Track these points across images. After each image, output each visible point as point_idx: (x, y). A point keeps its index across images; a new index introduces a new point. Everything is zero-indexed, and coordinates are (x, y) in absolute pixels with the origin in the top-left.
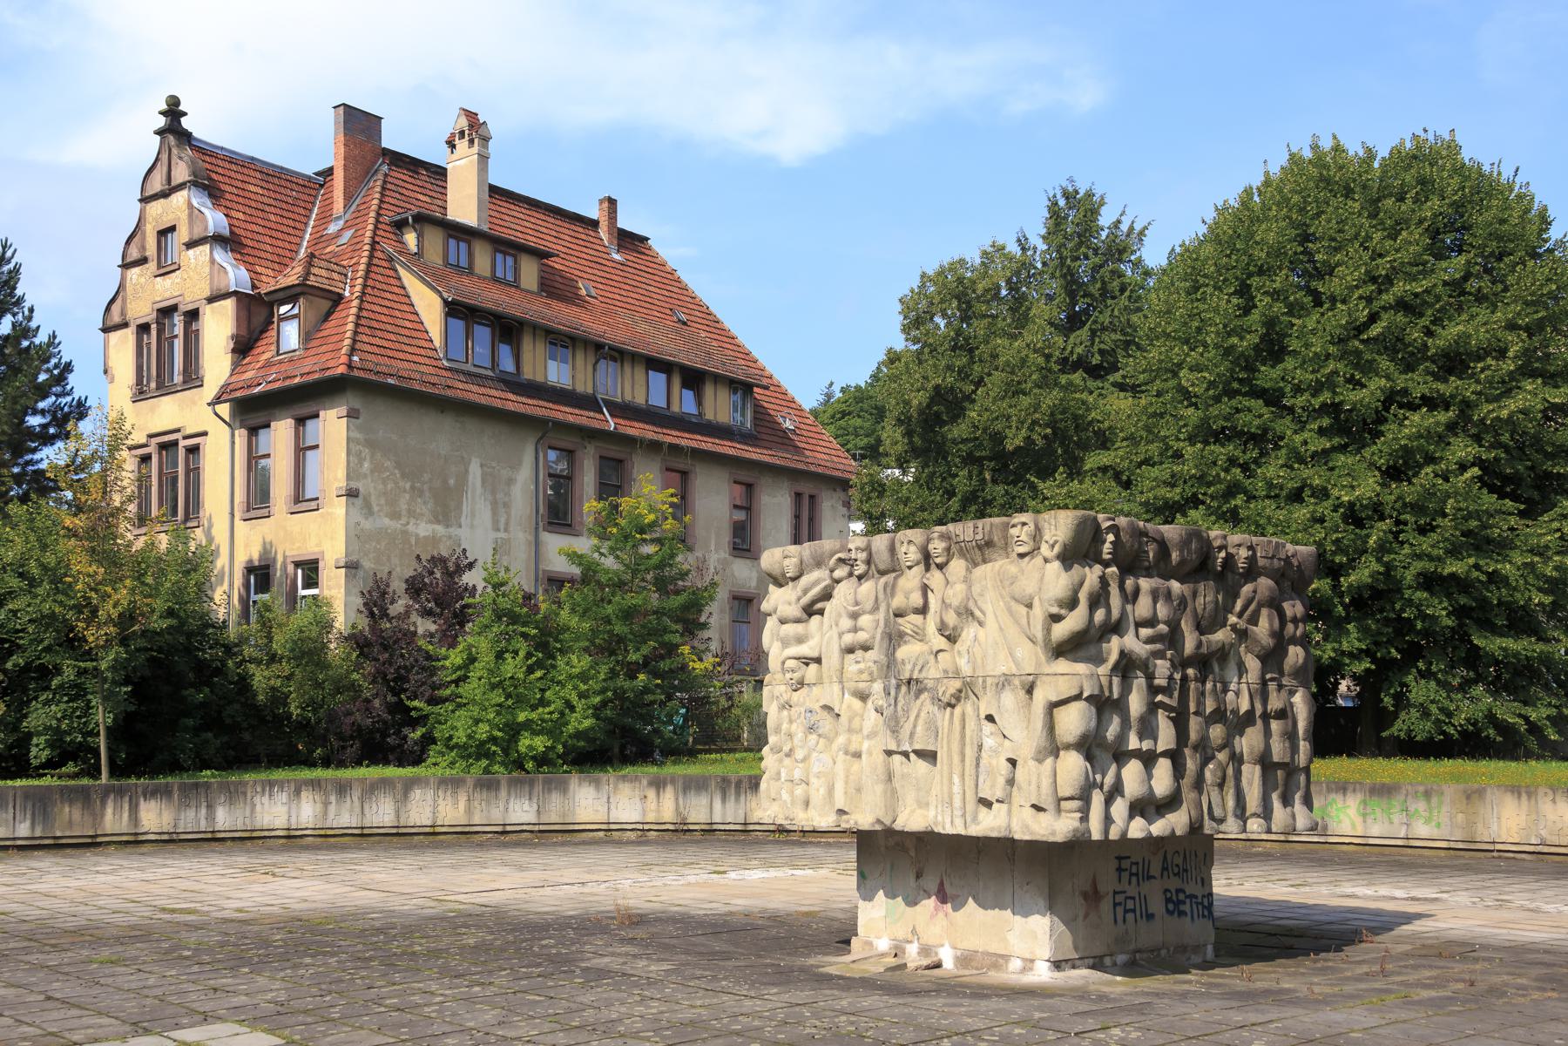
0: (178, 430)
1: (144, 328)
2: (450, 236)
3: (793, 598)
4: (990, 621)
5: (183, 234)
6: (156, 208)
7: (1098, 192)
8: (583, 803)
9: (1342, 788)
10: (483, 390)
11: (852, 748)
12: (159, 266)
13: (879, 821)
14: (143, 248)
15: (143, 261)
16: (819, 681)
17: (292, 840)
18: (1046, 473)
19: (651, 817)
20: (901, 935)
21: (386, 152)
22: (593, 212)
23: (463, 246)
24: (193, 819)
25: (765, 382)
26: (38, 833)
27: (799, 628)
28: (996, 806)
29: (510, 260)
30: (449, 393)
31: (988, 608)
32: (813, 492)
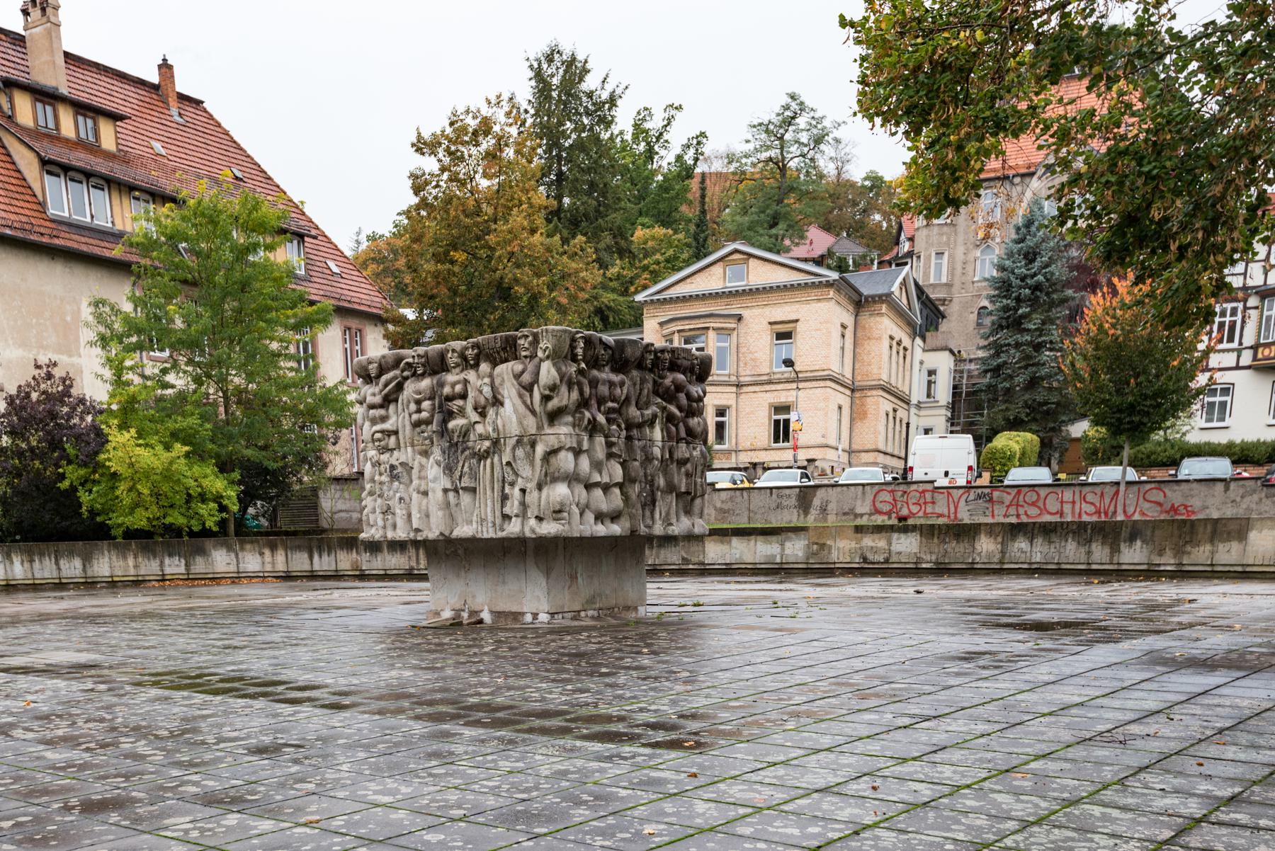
3: (377, 390)
4: (507, 403)
8: (219, 558)
10: (83, 240)
11: (422, 489)
13: (442, 534)
16: (398, 447)
18: (694, 408)
19: (268, 568)
20: (458, 606)
22: (154, 78)
25: (314, 232)
27: (382, 412)
28: (514, 519)
29: (90, 122)
30: (56, 241)
31: (506, 393)
32: (360, 327)
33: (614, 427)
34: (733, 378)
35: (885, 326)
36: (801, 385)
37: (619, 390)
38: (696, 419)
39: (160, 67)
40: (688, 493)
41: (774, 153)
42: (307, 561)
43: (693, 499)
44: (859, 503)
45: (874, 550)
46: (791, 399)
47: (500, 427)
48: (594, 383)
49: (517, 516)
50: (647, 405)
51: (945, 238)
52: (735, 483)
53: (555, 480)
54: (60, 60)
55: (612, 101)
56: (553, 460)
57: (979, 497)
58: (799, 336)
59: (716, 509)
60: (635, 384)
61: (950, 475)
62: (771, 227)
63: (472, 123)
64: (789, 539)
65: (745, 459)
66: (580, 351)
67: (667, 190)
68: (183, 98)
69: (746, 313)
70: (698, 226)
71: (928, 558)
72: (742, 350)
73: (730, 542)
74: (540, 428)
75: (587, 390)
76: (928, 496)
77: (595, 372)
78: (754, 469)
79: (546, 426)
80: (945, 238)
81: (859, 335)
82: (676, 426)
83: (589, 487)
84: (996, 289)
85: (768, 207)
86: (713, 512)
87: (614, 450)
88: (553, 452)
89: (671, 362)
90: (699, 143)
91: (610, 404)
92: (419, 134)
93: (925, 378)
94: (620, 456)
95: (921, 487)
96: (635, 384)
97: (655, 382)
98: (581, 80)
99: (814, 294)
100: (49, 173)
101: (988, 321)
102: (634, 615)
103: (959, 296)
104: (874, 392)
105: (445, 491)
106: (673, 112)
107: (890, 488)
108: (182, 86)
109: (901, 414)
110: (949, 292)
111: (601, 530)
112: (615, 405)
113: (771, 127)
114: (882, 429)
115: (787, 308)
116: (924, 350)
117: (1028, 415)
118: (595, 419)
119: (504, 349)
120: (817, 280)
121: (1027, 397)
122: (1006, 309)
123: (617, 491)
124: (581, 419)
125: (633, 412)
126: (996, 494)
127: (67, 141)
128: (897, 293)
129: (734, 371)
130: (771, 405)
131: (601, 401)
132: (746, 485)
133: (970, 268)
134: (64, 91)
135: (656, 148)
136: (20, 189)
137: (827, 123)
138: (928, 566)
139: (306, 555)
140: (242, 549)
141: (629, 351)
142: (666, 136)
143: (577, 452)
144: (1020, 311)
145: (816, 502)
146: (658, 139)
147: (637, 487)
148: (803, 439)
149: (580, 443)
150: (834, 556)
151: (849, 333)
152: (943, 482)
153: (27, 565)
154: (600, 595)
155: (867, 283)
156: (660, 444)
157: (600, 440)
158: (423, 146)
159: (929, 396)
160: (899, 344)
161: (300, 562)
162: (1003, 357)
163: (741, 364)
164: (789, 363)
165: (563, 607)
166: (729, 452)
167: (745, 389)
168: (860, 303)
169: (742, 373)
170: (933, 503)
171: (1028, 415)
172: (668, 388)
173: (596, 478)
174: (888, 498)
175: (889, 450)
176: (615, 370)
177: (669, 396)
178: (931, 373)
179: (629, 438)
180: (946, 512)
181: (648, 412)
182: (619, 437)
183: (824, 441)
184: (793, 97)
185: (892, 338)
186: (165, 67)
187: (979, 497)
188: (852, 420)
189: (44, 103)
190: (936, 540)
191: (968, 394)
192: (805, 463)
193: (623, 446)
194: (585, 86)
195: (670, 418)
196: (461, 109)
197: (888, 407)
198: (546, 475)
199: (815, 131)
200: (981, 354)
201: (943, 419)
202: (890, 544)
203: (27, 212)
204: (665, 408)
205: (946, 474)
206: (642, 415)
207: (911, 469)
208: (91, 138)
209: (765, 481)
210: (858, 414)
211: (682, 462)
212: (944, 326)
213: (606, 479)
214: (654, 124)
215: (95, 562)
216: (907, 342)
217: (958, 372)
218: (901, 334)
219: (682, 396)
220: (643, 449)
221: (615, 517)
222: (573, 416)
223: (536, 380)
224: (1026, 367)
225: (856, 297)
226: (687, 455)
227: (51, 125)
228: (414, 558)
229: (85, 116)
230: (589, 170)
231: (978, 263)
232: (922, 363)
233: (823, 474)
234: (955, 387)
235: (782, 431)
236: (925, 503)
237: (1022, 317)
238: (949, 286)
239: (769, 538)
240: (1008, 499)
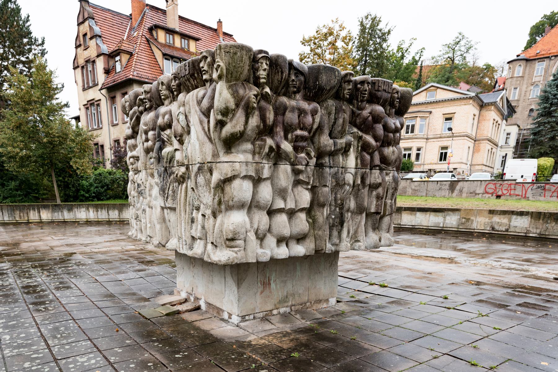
0: (94, 99)
1: (83, 67)
2: (167, 33)
5: (89, 36)
6: (82, 27)
7: (378, 16)
9: (319, 142)
12: (85, 47)
14: (80, 41)
15: (80, 45)
17: (88, 223)
18: (390, 138)
21: (147, 5)
22: (215, 27)
23: (171, 36)
24: (103, 215)
26: (11, 219)
33: (303, 155)
34: (425, 136)
35: (492, 115)
36: (454, 138)
37: (309, 119)
38: (391, 149)
39: (218, 22)
40: (377, 213)
41: (451, 55)
43: (382, 218)
44: (478, 188)
45: (500, 224)
46: (448, 144)
47: (189, 155)
48: (281, 110)
49: (200, 239)
50: (342, 134)
51: (518, 82)
52: (421, 178)
53: (230, 208)
54: (177, 18)
55: (389, 32)
56: (227, 189)
57: (539, 187)
58: (455, 119)
59: (412, 189)
60: (329, 114)
61: (524, 177)
62: (446, 82)
63: (325, 31)
64: (449, 215)
65: (426, 168)
66: (262, 74)
67: (407, 69)
68: (225, 34)
69: (433, 110)
70: (418, 81)
71: (535, 231)
72: (430, 125)
73: (416, 214)
74: (215, 155)
75: (270, 116)
76: (513, 187)
77: (284, 99)
78: (430, 172)
79: (221, 153)
80: (518, 82)
81: (480, 119)
82: (371, 155)
83: (271, 213)
84: (542, 100)
85: (445, 75)
86: (410, 190)
87: (301, 177)
88: (228, 180)
89: (370, 94)
90: (422, 52)
91: (299, 132)
92: (304, 38)
93: (505, 136)
94: (308, 183)
95: (510, 182)
96: (329, 114)
97: (353, 113)
98: (378, 25)
99: (465, 101)
100: (166, 59)
101: (535, 114)
102: (325, 305)
103: (521, 104)
104: (484, 142)
105: (163, 208)
106: (413, 41)
107: (494, 182)
108: (225, 30)
109: (494, 150)
110: (518, 103)
111: (283, 252)
112: (305, 133)
113: (450, 45)
114: (486, 156)
115: (451, 108)
116: (506, 125)
117: (550, 151)
118: (278, 147)
119: (192, 75)
120: (465, 96)
121: (551, 143)
122: (545, 108)
123: (303, 216)
124: (261, 147)
125: (325, 140)
126: (547, 187)
127: (177, 48)
128: (499, 102)
129: (426, 133)
130: (440, 147)
131: (288, 129)
132: (427, 179)
133: (528, 94)
134: (177, 30)
135: (405, 55)
136: (154, 65)
137: (472, 43)
138: (534, 235)
141: (324, 78)
142: (409, 50)
143: (257, 181)
144: (552, 109)
145: (458, 188)
146: (406, 51)
147: (326, 211)
148: (452, 160)
149: (258, 171)
150: (474, 226)
151: (476, 118)
152: (520, 180)
153: (95, 213)
154: (293, 295)
155: (486, 98)
156: (353, 171)
157: (285, 168)
158: (304, 42)
159: (506, 143)
160: (497, 122)
162: (542, 128)
163: (429, 130)
164: (450, 129)
165: (254, 309)
166: (421, 165)
167: (430, 140)
168: (482, 106)
169: (429, 133)
170: (515, 189)
171: (550, 151)
172: (366, 119)
173: (280, 204)
174: (493, 187)
175: (488, 165)
176: (307, 98)
177: (366, 126)
178: (508, 134)
179: (319, 166)
180: (521, 194)
181: (342, 142)
182: (307, 162)
183: (461, 161)
184: (460, 34)
185: (494, 120)
186: (220, 22)
187: (539, 187)
188: (473, 152)
189: (169, 34)
190: (541, 221)
191: (522, 143)
192: (452, 170)
193: (311, 173)
194: (379, 27)
195: (365, 147)
196: (321, 26)
197: (490, 147)
198: (220, 203)
199: (467, 46)
200: (529, 127)
201: (512, 152)
202: (510, 221)
203: (156, 74)
204: (360, 138)
205: (522, 176)
206: (335, 144)
207: (505, 174)
208: (186, 47)
209: (436, 177)
210: (476, 150)
211: (374, 187)
212: (515, 116)
213: (291, 205)
214: (405, 46)
215: (124, 212)
216: (500, 122)
217: (519, 134)
218: (498, 118)
219: (379, 128)
220: (335, 176)
221: (300, 239)
222: (253, 143)
223: (211, 107)
224: (552, 131)
225: (481, 103)
226: (379, 181)
227: (171, 42)
229: (185, 39)
230: (377, 59)
231: (532, 91)
232: (504, 130)
233: (459, 174)
234: (517, 140)
235: (443, 157)
236: (511, 190)
237: (552, 111)
238: (518, 100)
239: (437, 214)
240: (553, 189)
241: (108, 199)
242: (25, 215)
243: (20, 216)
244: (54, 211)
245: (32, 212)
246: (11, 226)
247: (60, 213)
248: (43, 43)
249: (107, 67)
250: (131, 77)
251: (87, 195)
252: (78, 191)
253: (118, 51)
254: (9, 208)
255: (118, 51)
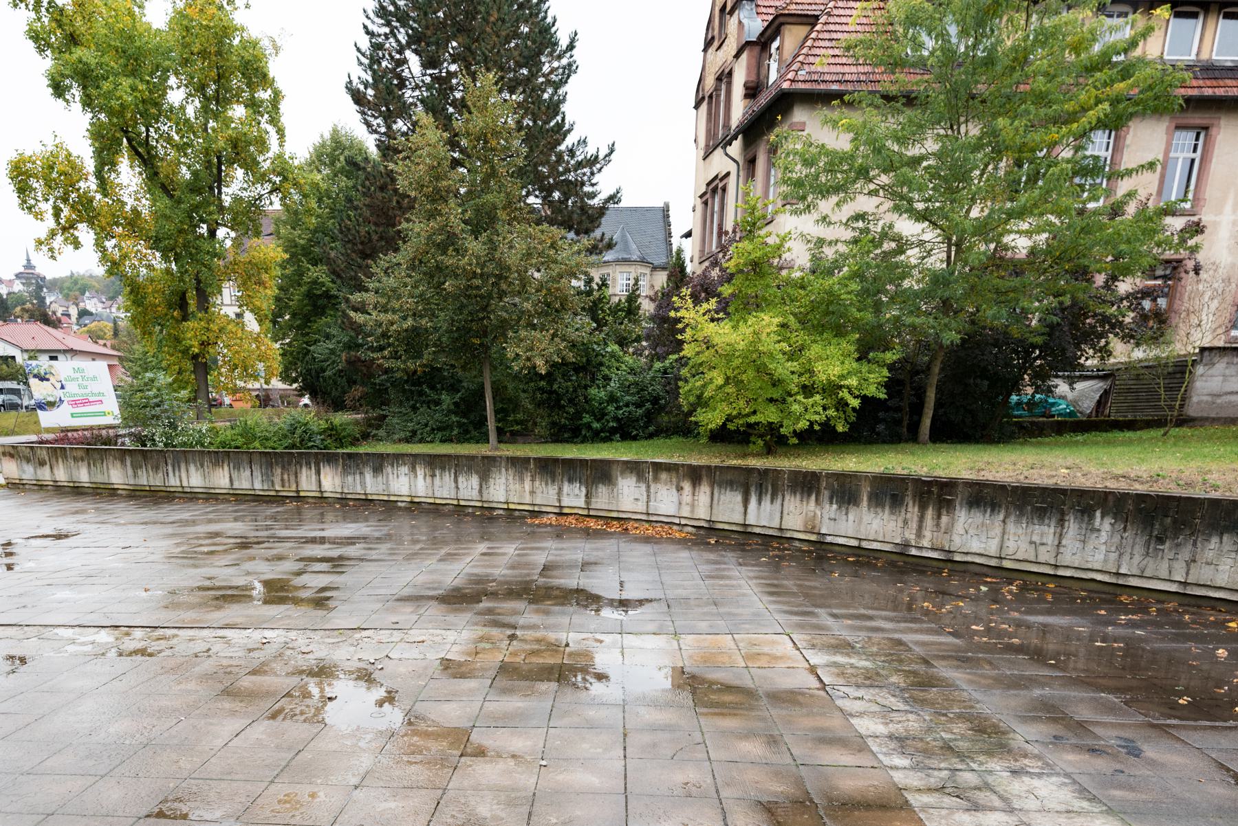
8: (626, 491)
19: (686, 512)
42: (740, 508)
139: (738, 498)
140: (656, 479)
153: (429, 479)
161: (729, 509)
228: (914, 525)
241: (599, 437)
242: (292, 478)
243: (282, 480)
244: (346, 471)
245: (304, 469)
246: (1104, 524)
247: (358, 477)
248: (571, 47)
249: (753, 78)
250: (786, 85)
251: (596, 425)
252: (578, 415)
253: (777, 22)
254: (264, 460)
255: (777, 22)
